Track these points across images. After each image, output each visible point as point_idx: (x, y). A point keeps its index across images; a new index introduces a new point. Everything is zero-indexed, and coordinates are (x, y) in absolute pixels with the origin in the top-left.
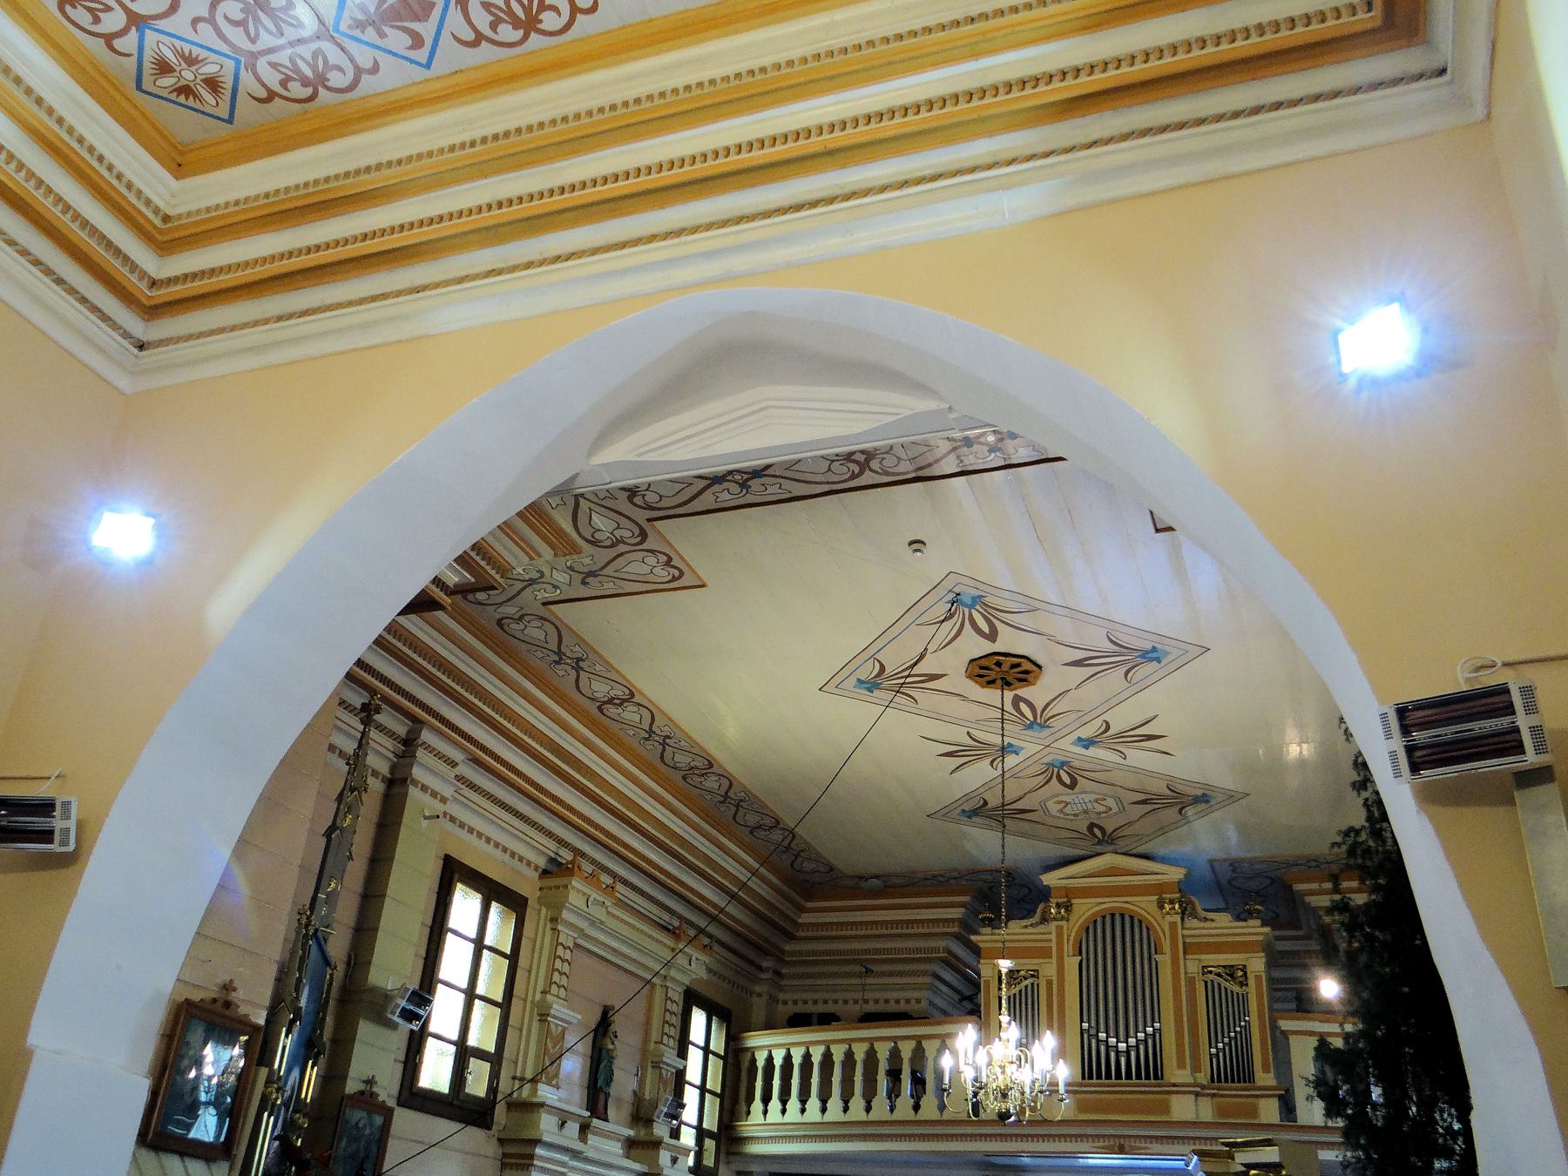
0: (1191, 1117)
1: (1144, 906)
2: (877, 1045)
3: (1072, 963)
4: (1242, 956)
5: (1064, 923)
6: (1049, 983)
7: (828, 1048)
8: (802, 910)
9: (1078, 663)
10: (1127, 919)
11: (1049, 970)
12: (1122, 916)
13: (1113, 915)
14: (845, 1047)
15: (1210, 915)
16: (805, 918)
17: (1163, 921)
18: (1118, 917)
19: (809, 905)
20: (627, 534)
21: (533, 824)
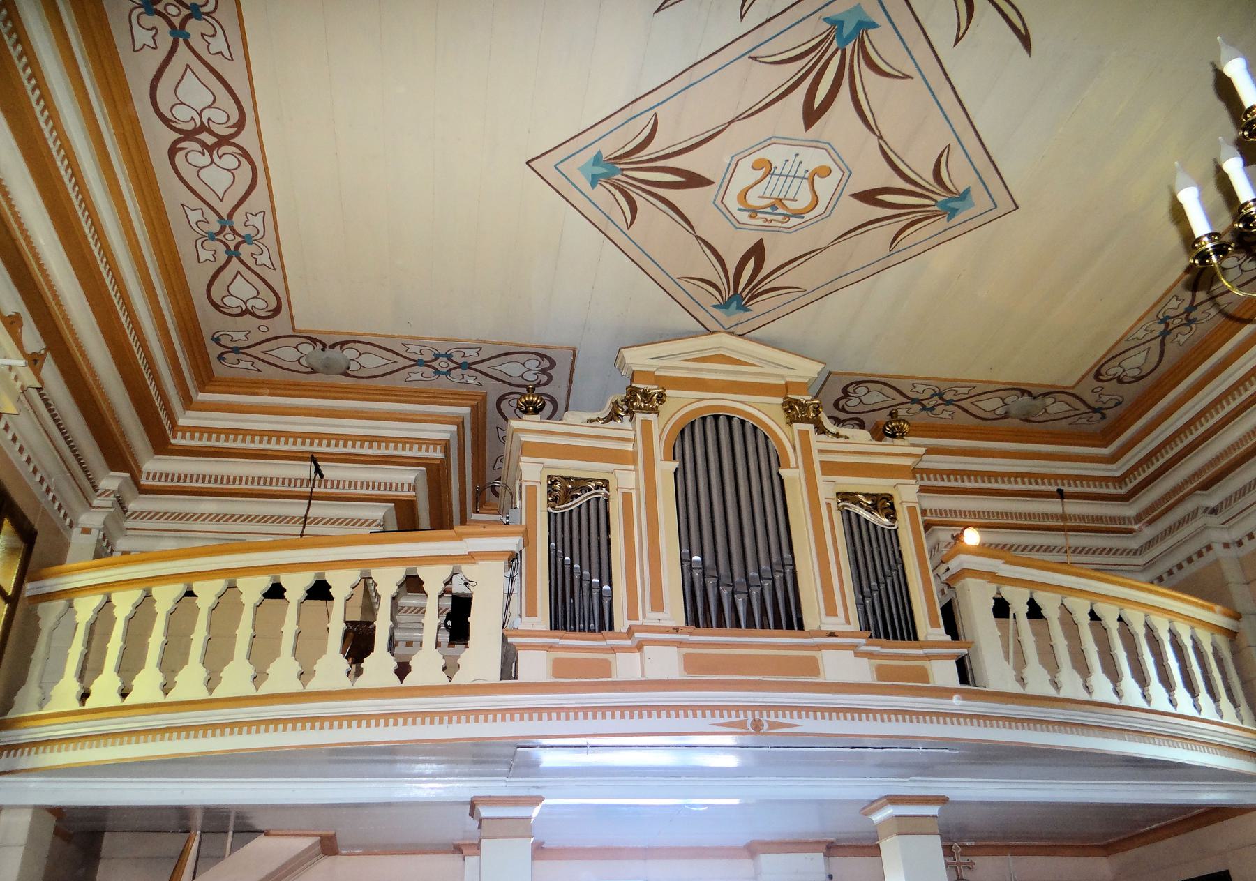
0: (637, 676)
1: (765, 412)
2: (376, 574)
3: (666, 469)
4: (893, 481)
5: (651, 417)
6: (627, 498)
7: (366, 578)
8: (188, 403)
9: (693, 180)
10: (736, 424)
11: (626, 479)
12: (730, 418)
13: (716, 417)
14: (354, 575)
15: (843, 431)
16: (186, 419)
17: (785, 434)
18: (722, 421)
19: (202, 397)
20: (259, 304)
21: (247, 519)
